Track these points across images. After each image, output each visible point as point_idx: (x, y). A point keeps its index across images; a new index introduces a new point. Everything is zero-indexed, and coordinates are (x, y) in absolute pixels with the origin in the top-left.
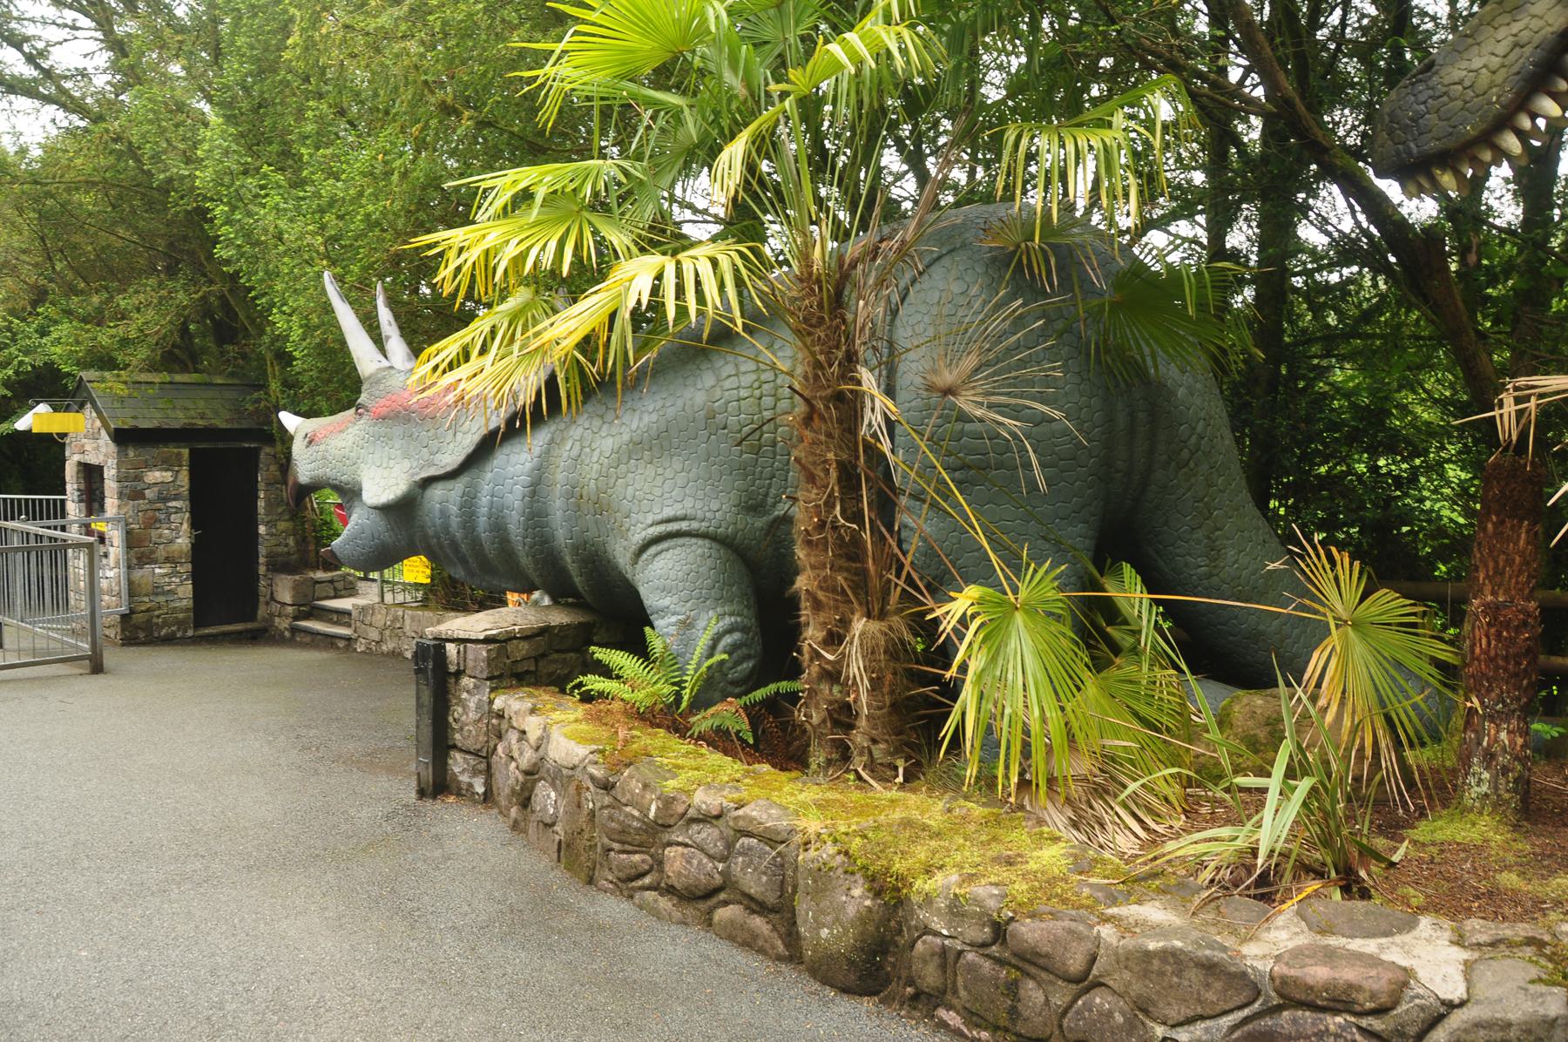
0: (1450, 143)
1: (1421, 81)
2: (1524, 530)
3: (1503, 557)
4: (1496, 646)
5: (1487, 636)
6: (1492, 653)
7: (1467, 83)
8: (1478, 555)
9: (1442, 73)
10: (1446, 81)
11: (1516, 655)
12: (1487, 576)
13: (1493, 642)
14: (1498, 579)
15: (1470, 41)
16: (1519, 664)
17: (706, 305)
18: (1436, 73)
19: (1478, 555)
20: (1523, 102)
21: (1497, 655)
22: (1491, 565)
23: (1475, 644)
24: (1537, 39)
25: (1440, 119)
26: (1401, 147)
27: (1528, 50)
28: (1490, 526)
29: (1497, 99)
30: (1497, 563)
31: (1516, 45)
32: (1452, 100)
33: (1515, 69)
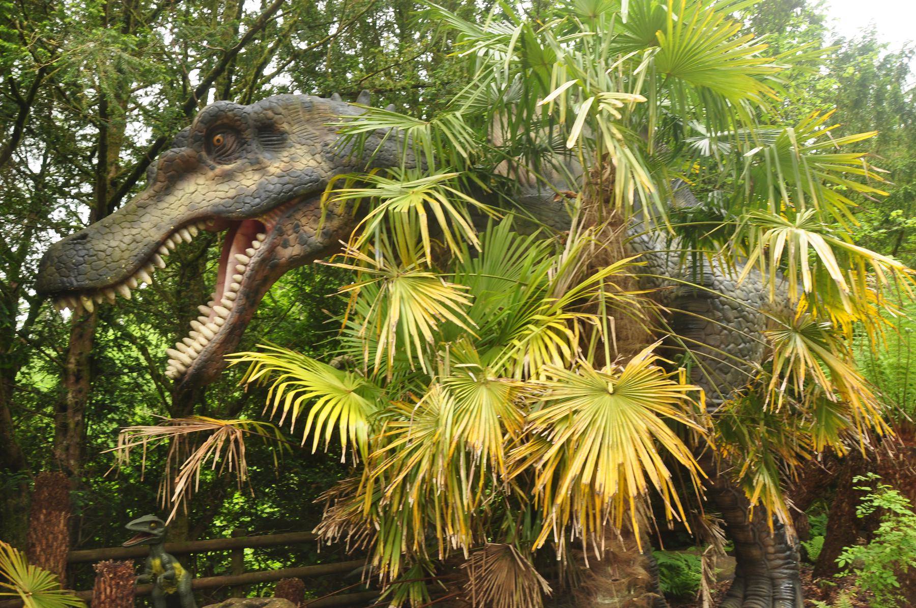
0: (99, 285)
1: (80, 243)
2: (62, 518)
3: (51, 536)
4: (116, 592)
5: (110, 586)
6: (113, 597)
7: (108, 253)
8: (35, 536)
9: (94, 242)
10: (97, 248)
11: (128, 595)
12: (42, 550)
13: (114, 590)
14: (49, 551)
15: (108, 230)
16: (128, 600)
17: (345, 180)
18: (89, 241)
19: (35, 536)
20: (135, 272)
21: (117, 597)
22: (44, 542)
23: (101, 593)
24: (145, 241)
25: (92, 269)
26: (65, 279)
27: (141, 245)
28: (42, 517)
29: (126, 265)
30: (47, 540)
31: (134, 241)
32: (100, 260)
33: (134, 253)
